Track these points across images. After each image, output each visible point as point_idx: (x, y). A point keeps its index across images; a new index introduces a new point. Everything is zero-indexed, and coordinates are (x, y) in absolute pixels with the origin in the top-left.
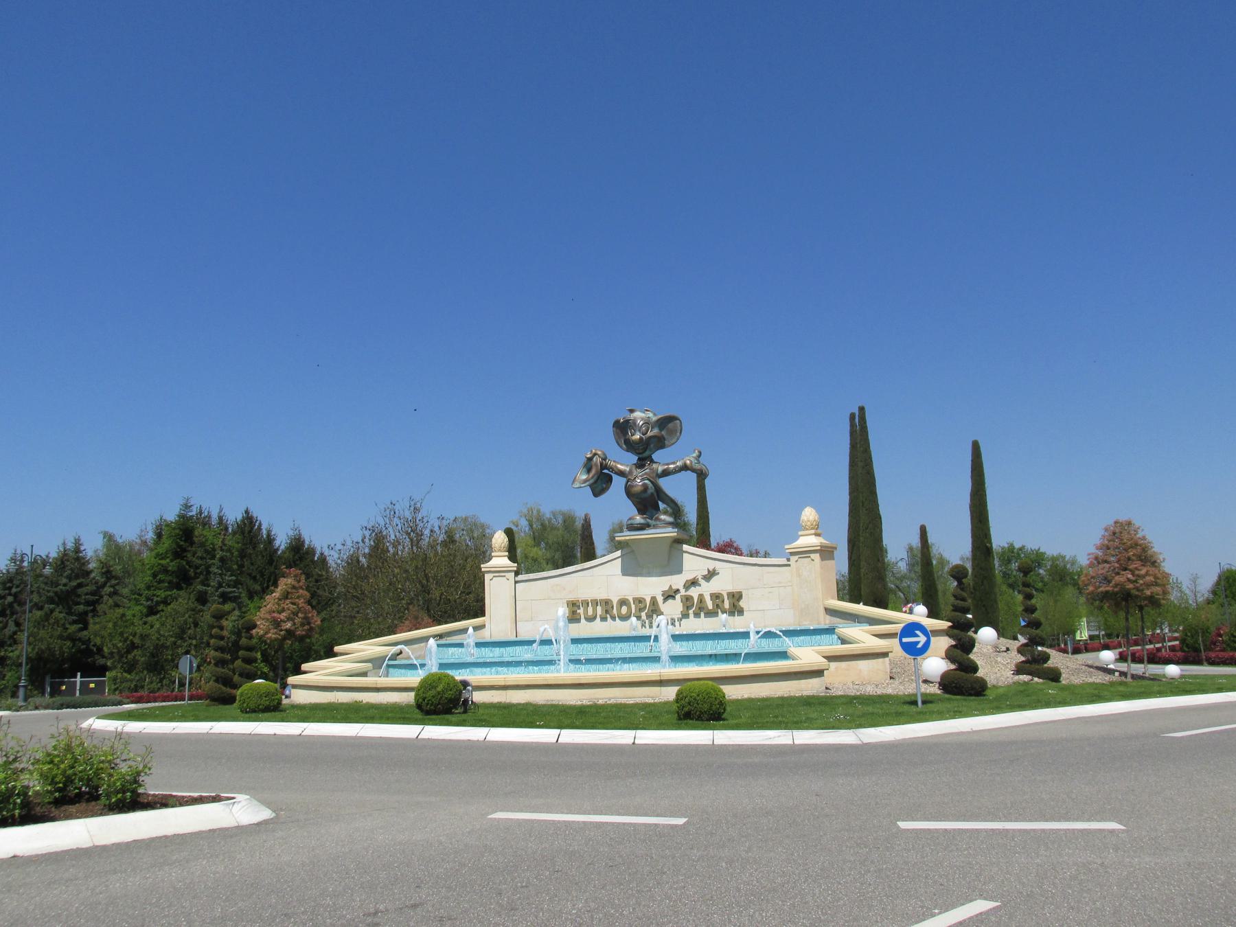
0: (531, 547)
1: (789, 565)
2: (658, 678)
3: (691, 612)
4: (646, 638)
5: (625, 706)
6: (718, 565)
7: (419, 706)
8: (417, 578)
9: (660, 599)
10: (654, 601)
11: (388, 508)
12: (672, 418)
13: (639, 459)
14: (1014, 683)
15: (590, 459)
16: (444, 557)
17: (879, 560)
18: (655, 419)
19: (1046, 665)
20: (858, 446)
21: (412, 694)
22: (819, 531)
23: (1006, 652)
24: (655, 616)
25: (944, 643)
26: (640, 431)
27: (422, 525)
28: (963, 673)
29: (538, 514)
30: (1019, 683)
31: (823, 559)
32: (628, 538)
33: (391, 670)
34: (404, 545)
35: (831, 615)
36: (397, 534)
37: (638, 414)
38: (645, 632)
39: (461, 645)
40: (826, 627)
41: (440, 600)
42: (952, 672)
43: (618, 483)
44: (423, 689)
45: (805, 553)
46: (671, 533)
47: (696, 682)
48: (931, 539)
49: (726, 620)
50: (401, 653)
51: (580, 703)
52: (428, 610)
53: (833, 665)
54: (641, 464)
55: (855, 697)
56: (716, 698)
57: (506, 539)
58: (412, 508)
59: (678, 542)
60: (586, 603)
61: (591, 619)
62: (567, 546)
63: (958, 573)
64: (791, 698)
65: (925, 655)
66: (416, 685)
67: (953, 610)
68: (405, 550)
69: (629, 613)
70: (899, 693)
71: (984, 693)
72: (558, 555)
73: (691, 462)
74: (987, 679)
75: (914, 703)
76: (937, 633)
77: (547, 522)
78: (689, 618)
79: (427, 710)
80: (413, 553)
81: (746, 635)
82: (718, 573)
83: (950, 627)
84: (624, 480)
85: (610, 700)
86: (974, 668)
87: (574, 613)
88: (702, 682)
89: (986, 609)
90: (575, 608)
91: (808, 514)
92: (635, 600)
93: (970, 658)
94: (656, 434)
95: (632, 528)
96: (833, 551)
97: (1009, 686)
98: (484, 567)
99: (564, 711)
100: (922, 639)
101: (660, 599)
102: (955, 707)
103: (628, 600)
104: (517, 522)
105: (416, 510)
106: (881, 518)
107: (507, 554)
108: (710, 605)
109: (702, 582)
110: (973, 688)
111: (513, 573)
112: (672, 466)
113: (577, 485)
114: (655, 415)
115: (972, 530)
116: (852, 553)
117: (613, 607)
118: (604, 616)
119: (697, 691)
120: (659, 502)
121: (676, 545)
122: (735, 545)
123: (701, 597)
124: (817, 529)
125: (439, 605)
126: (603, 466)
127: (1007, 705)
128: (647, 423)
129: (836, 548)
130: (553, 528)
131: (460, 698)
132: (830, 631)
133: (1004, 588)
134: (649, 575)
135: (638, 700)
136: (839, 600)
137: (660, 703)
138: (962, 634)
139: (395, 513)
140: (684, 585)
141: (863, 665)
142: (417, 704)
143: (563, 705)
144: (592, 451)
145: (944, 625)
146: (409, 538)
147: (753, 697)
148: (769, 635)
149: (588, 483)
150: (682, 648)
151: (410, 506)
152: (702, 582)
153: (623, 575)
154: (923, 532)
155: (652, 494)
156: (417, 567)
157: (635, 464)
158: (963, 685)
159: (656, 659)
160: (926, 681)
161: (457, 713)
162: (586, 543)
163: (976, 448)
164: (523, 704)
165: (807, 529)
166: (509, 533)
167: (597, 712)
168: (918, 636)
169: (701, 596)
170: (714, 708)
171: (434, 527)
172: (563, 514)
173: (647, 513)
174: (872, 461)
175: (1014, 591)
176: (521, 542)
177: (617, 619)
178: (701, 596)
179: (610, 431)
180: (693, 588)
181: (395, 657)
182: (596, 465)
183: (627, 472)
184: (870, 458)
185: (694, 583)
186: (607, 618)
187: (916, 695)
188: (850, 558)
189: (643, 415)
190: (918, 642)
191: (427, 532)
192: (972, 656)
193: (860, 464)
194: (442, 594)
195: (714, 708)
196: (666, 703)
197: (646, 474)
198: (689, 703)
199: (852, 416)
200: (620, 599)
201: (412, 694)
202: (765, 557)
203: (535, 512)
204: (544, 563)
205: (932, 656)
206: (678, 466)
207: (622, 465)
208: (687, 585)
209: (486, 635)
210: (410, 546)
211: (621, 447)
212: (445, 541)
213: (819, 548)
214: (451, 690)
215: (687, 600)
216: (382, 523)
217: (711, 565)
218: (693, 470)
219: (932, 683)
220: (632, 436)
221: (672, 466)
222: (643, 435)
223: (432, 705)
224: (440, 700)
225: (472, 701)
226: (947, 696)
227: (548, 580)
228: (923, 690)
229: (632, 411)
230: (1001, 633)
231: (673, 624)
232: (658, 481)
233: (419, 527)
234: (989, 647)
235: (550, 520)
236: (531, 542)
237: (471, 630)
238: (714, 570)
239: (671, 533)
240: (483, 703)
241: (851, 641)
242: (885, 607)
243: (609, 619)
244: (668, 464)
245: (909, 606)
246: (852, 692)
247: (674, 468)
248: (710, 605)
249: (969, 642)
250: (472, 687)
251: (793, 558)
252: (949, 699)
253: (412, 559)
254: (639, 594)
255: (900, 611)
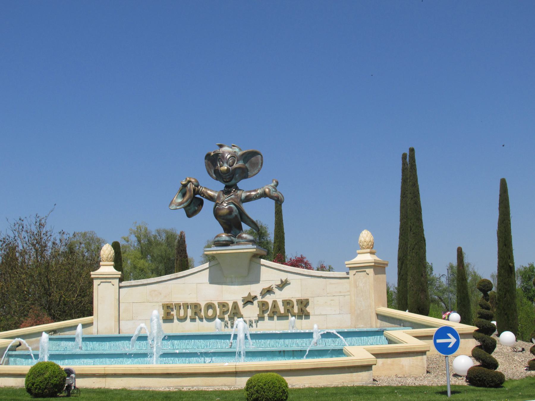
0: (139, 259)
1: (348, 278)
2: (234, 370)
3: (266, 315)
4: (227, 337)
5: (206, 392)
6: (290, 277)
7: (29, 390)
8: (41, 283)
9: (240, 304)
10: (235, 305)
11: (17, 223)
12: (254, 154)
13: (226, 187)
14: (527, 377)
15: (185, 186)
16: (63, 265)
17: (422, 275)
18: (240, 153)
19: (496, 370)
20: (408, 180)
21: (24, 379)
22: (373, 250)
23: (521, 351)
24: (236, 318)
25: (472, 343)
26: (227, 163)
27: (46, 238)
28: (485, 369)
29: (146, 232)
30: (531, 377)
31: (376, 273)
32: (214, 252)
33: (12, 359)
34: (30, 255)
35: (381, 320)
36: (25, 245)
37: (226, 149)
38: (227, 331)
39: (73, 339)
40: (377, 329)
41: (60, 301)
42: (476, 368)
43: (208, 206)
44: (32, 376)
45: (361, 268)
46: (251, 249)
47: (263, 374)
48: (466, 261)
49: (294, 321)
50: (20, 344)
51: (167, 389)
52: (49, 309)
53: (380, 361)
54: (227, 191)
55: (397, 388)
56: (279, 387)
57: (113, 251)
58: (38, 224)
59: (257, 256)
60: (178, 306)
61: (182, 320)
62: (169, 259)
63: (484, 286)
64: (344, 388)
65: (455, 354)
66: (26, 372)
67: (480, 317)
68: (31, 259)
69: (214, 316)
70: (434, 385)
71: (502, 385)
72: (161, 267)
73: (270, 190)
74: (505, 374)
75: (445, 393)
76: (466, 336)
77: (153, 239)
78: (273, 320)
79: (36, 393)
80: (38, 261)
81: (309, 335)
82: (289, 284)
83: (476, 331)
84: (213, 204)
85: (193, 387)
86: (495, 365)
87: (168, 314)
88: (268, 374)
89: (508, 317)
90: (169, 310)
91: (365, 235)
92: (219, 304)
93: (491, 357)
94: (242, 166)
95: (219, 244)
96: (385, 267)
97: (522, 380)
98: (93, 274)
99: (152, 396)
100: (453, 340)
101: (240, 304)
102: (478, 396)
103: (214, 304)
104: (128, 238)
105: (41, 225)
106: (425, 240)
107: (113, 263)
108: (282, 310)
109: (276, 290)
110: (493, 381)
111: (118, 280)
112: (253, 193)
113: (173, 207)
114: (240, 150)
115: (499, 253)
116: (401, 269)
117: (201, 310)
118: (193, 317)
119: (264, 381)
120: (242, 222)
121: (255, 260)
122: (305, 260)
123: (275, 303)
124: (372, 248)
125: (58, 305)
126: (196, 192)
127: (520, 395)
128: (233, 156)
129: (387, 265)
130: (158, 244)
131: (64, 384)
132: (380, 333)
133: (525, 300)
134: (232, 283)
135: (216, 388)
136: (388, 307)
137: (234, 390)
138: (486, 336)
139: (23, 227)
140: (261, 293)
141: (405, 361)
142: (27, 388)
143: (153, 391)
144: (186, 179)
145: (472, 329)
146: (35, 249)
147: (313, 386)
148: (327, 335)
149: (182, 206)
150: (168, 346)
151: (36, 222)
152: (276, 290)
153: (210, 283)
154: (460, 253)
155: (236, 216)
156: (40, 274)
157: (222, 191)
158: (485, 378)
159: (231, 354)
160: (455, 375)
161: (61, 396)
162: (181, 256)
163: (503, 185)
164: (120, 390)
165: (364, 249)
166: (116, 246)
167: (180, 398)
168: (449, 338)
169: (275, 302)
170: (278, 395)
171: (56, 240)
172: (166, 232)
173: (232, 232)
174: (419, 193)
175: (532, 303)
176: (130, 255)
177: (204, 320)
178: (275, 302)
179: (202, 162)
180: (268, 295)
181: (14, 348)
182: (190, 190)
183: (216, 197)
184: (418, 191)
185: (269, 291)
186: (288, 316)
187: (446, 386)
188: (399, 274)
189: (230, 150)
190: (449, 343)
191: (50, 244)
192: (493, 355)
193: (409, 196)
194: (61, 297)
195: (278, 395)
196: (240, 391)
197: (231, 199)
198: (257, 391)
199: (404, 156)
200: (207, 304)
201: (24, 379)
202: (329, 271)
203: (143, 230)
204: (150, 272)
205: (459, 355)
206: (258, 193)
207: (211, 191)
208: (263, 293)
209: (93, 331)
210: (35, 256)
211: (211, 176)
212: (66, 252)
213: (373, 264)
214: (56, 377)
215: (263, 306)
216: (12, 235)
217: (284, 276)
218: (271, 197)
219: (461, 376)
220: (220, 167)
221: (253, 193)
222: (230, 166)
223: (39, 389)
224: (46, 385)
225: (75, 387)
226: (472, 387)
227: (148, 286)
228: (453, 382)
229: (221, 146)
230: (519, 336)
231: (251, 325)
232: (241, 205)
233: (43, 240)
234: (509, 348)
235: (155, 237)
236: (139, 255)
237: (80, 327)
238: (286, 281)
239: (251, 249)
240: (85, 389)
241: (396, 341)
242: (426, 314)
243: (197, 320)
244: (250, 192)
245: (448, 313)
246: (394, 384)
247: (255, 195)
248: (282, 310)
249: (491, 343)
250: (75, 374)
251: (352, 272)
252: (473, 390)
253: (37, 267)
254: (224, 299)
255: (441, 317)
